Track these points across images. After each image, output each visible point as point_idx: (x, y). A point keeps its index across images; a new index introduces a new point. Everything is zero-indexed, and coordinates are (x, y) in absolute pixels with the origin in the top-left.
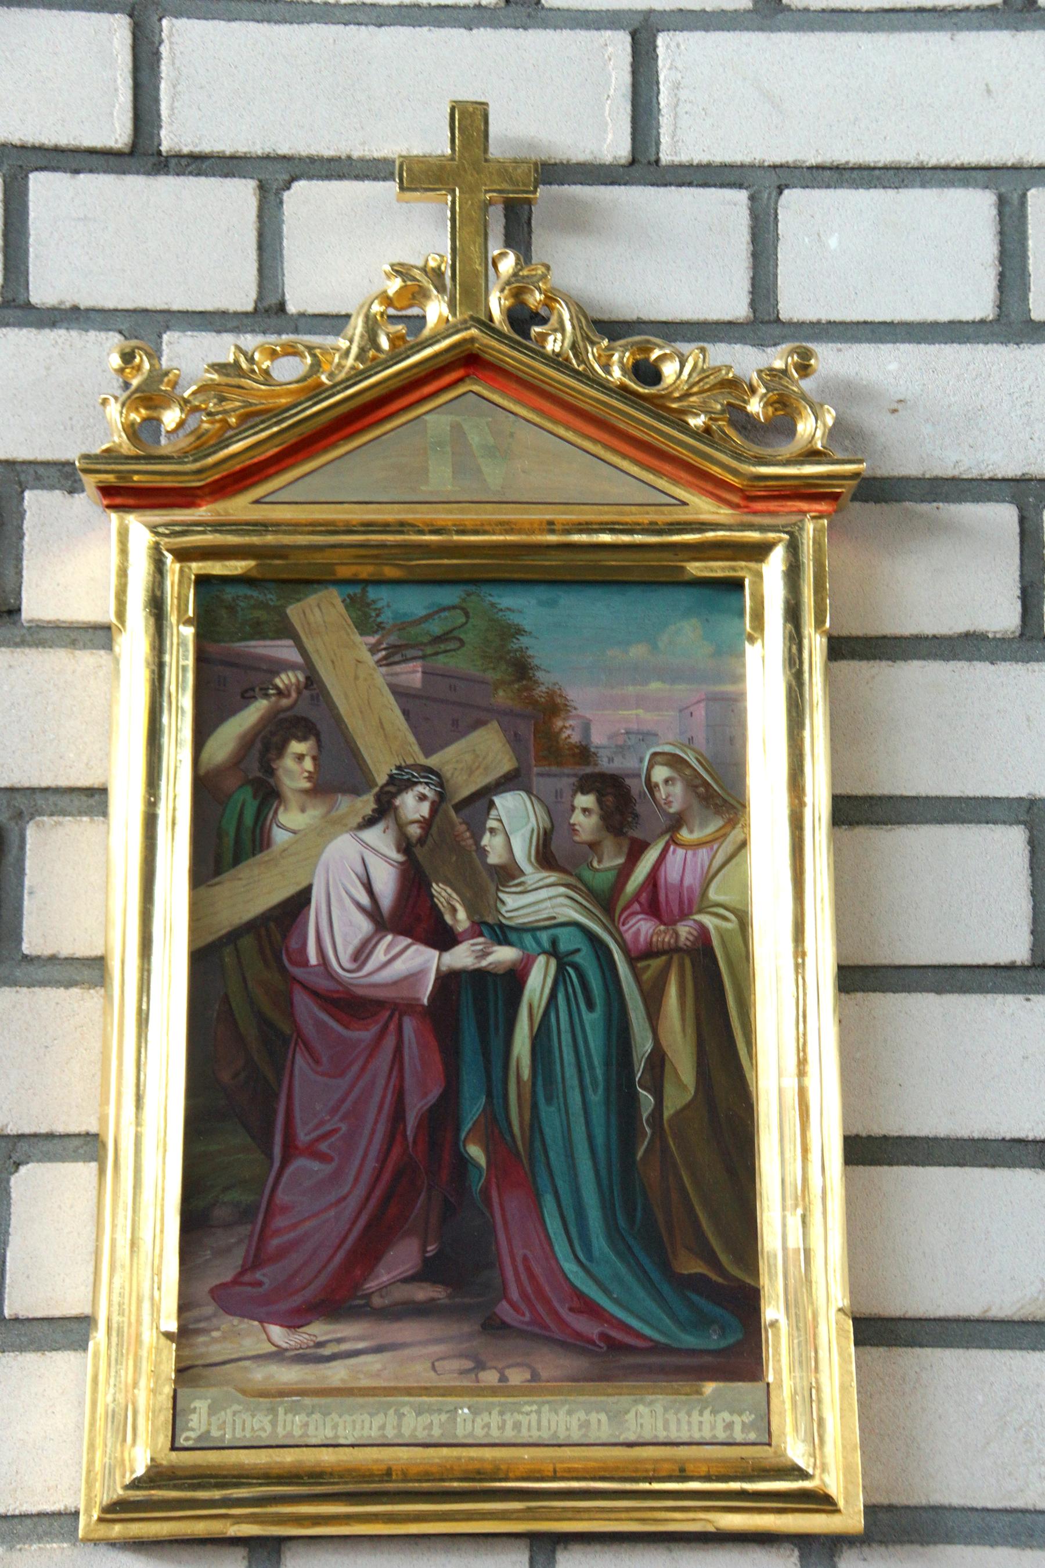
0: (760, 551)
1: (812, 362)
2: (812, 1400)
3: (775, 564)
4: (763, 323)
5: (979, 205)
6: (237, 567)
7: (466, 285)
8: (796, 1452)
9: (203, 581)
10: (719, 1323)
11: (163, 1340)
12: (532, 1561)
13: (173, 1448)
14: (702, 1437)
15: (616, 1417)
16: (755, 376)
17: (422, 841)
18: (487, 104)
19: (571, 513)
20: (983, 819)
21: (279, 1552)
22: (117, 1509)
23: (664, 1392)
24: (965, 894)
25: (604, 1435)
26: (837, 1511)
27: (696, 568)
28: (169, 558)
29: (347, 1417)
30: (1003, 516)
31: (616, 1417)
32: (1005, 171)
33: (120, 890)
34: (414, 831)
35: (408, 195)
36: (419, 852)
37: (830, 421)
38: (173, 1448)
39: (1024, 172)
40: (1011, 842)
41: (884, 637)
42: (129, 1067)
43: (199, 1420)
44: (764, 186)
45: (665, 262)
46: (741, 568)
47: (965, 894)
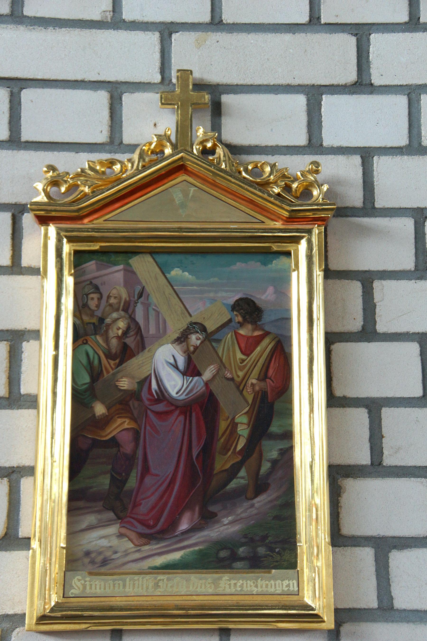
0: (296, 240)
1: (320, 168)
2: (314, 577)
5: (102, 97)
6: (96, 247)
8: (308, 601)
10: (273, 545)
11: (61, 549)
12: (221, 640)
13: (63, 597)
14: (267, 591)
15: (215, 583)
16: (299, 174)
17: (194, 352)
19: (125, 224)
20: (5, 332)
21: (229, 635)
22: (43, 619)
23: (227, 573)
24: (385, 369)
25: (210, 591)
26: (324, 622)
28: (65, 240)
29: (272, 582)
30: (407, 225)
31: (215, 583)
32: (17, 81)
33: (51, 372)
34: (192, 349)
35: (164, 106)
36: (193, 356)
37: (325, 189)
39: (70, 82)
40: (414, 348)
41: (351, 271)
42: (47, 440)
46: (291, 247)
47: (385, 369)
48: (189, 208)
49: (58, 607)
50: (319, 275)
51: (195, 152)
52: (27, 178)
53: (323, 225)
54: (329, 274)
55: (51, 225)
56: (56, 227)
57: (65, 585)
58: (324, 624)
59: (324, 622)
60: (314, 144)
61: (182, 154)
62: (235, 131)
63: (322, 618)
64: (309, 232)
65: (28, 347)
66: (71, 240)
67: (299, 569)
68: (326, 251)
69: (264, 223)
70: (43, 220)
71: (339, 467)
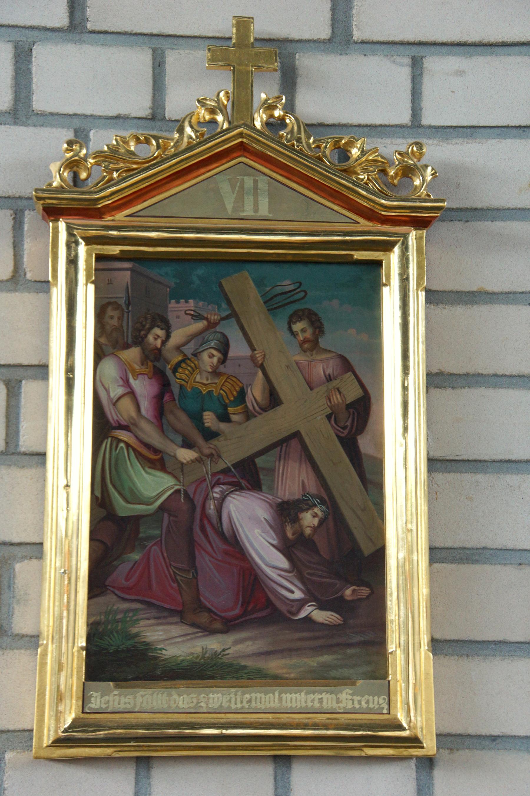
0: (388, 247)
3: (395, 256)
4: (416, 123)
7: (242, 103)
9: (99, 258)
13: (83, 712)
14: (101, 708)
18: (253, 18)
21: (289, 767)
26: (423, 747)
27: (358, 255)
38: (83, 712)
43: (97, 701)
44: (416, 52)
45: (351, 95)
48: (248, 210)
49: (75, 725)
50: (418, 300)
51: (258, 124)
52: (37, 157)
53: (357, 160)
54: (433, 297)
55: (61, 219)
56: (65, 222)
57: (84, 699)
58: (423, 750)
59: (423, 747)
60: (416, 123)
61: (242, 129)
62: (313, 105)
63: (421, 743)
64: (405, 236)
65: (29, 388)
66: (89, 241)
67: (390, 679)
68: (485, 45)
69: (359, 223)
70: (53, 212)
71: (440, 374)
